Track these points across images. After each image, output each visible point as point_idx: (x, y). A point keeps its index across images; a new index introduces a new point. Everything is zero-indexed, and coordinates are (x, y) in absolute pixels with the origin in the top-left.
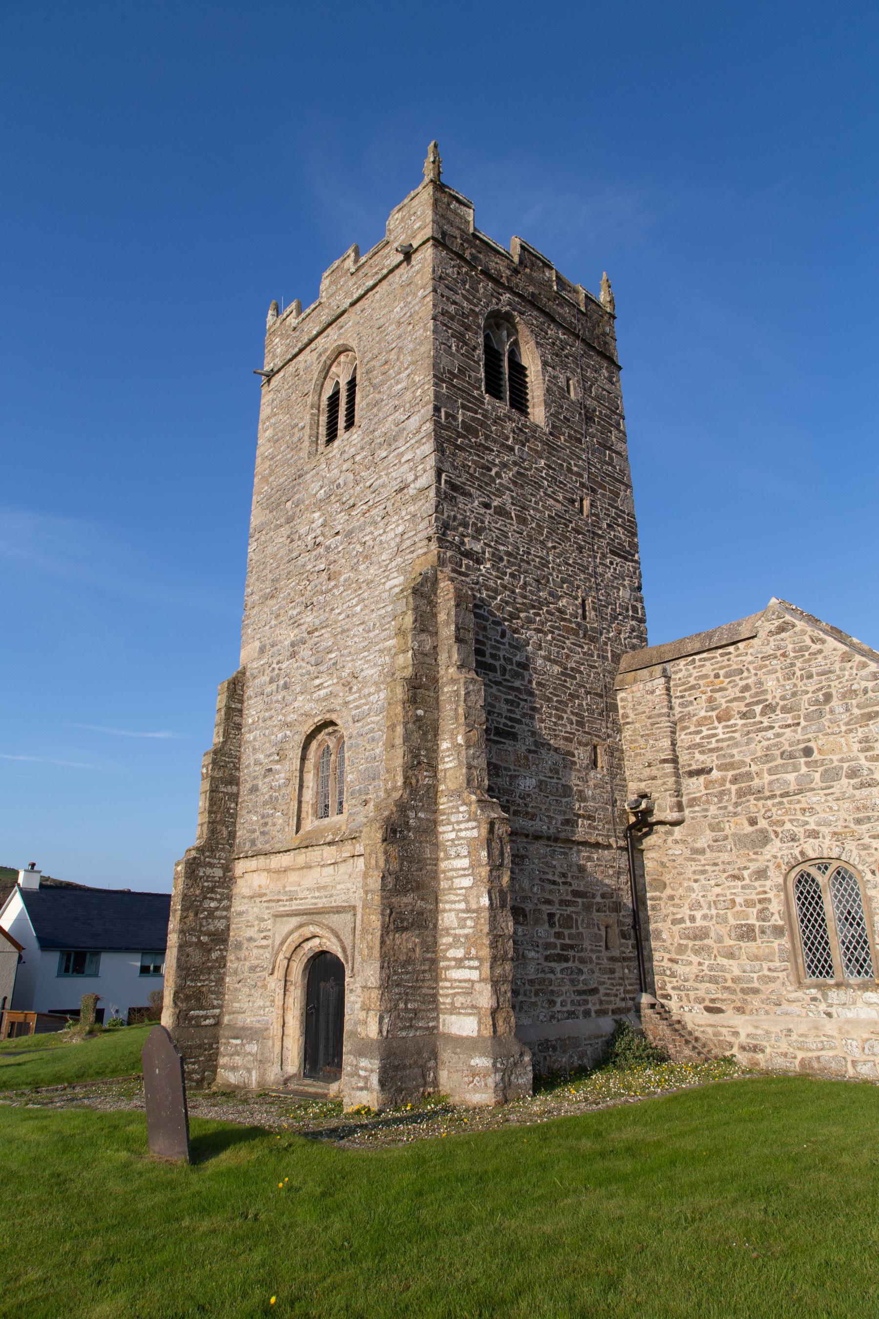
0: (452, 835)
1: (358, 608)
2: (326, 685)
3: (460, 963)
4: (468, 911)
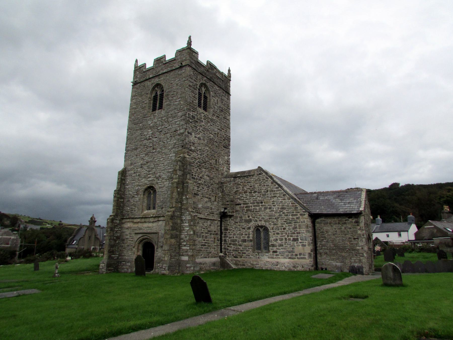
0: (185, 218)
1: (162, 159)
2: (151, 177)
3: (185, 246)
4: (187, 235)
